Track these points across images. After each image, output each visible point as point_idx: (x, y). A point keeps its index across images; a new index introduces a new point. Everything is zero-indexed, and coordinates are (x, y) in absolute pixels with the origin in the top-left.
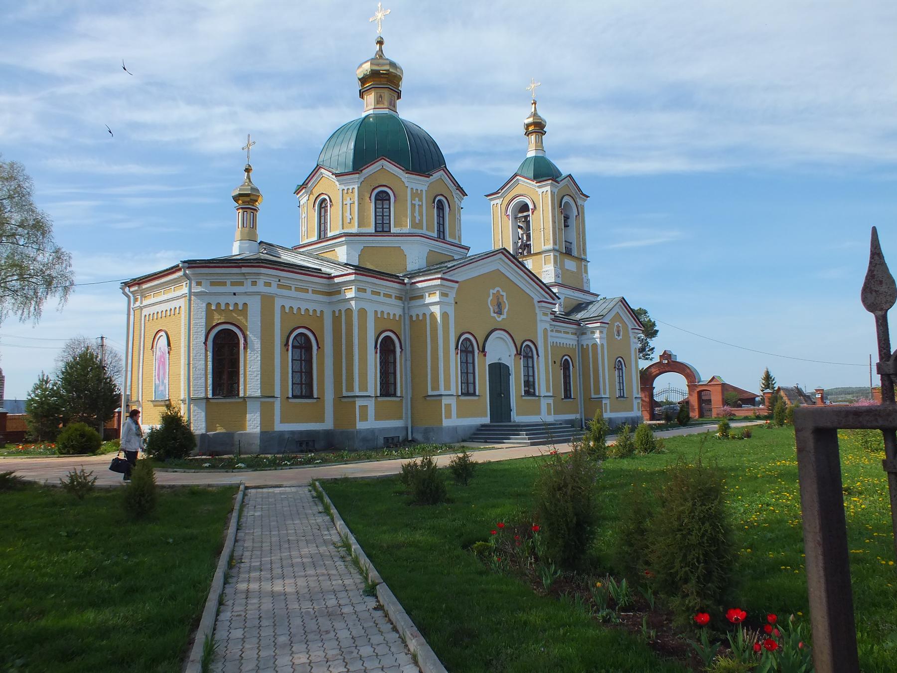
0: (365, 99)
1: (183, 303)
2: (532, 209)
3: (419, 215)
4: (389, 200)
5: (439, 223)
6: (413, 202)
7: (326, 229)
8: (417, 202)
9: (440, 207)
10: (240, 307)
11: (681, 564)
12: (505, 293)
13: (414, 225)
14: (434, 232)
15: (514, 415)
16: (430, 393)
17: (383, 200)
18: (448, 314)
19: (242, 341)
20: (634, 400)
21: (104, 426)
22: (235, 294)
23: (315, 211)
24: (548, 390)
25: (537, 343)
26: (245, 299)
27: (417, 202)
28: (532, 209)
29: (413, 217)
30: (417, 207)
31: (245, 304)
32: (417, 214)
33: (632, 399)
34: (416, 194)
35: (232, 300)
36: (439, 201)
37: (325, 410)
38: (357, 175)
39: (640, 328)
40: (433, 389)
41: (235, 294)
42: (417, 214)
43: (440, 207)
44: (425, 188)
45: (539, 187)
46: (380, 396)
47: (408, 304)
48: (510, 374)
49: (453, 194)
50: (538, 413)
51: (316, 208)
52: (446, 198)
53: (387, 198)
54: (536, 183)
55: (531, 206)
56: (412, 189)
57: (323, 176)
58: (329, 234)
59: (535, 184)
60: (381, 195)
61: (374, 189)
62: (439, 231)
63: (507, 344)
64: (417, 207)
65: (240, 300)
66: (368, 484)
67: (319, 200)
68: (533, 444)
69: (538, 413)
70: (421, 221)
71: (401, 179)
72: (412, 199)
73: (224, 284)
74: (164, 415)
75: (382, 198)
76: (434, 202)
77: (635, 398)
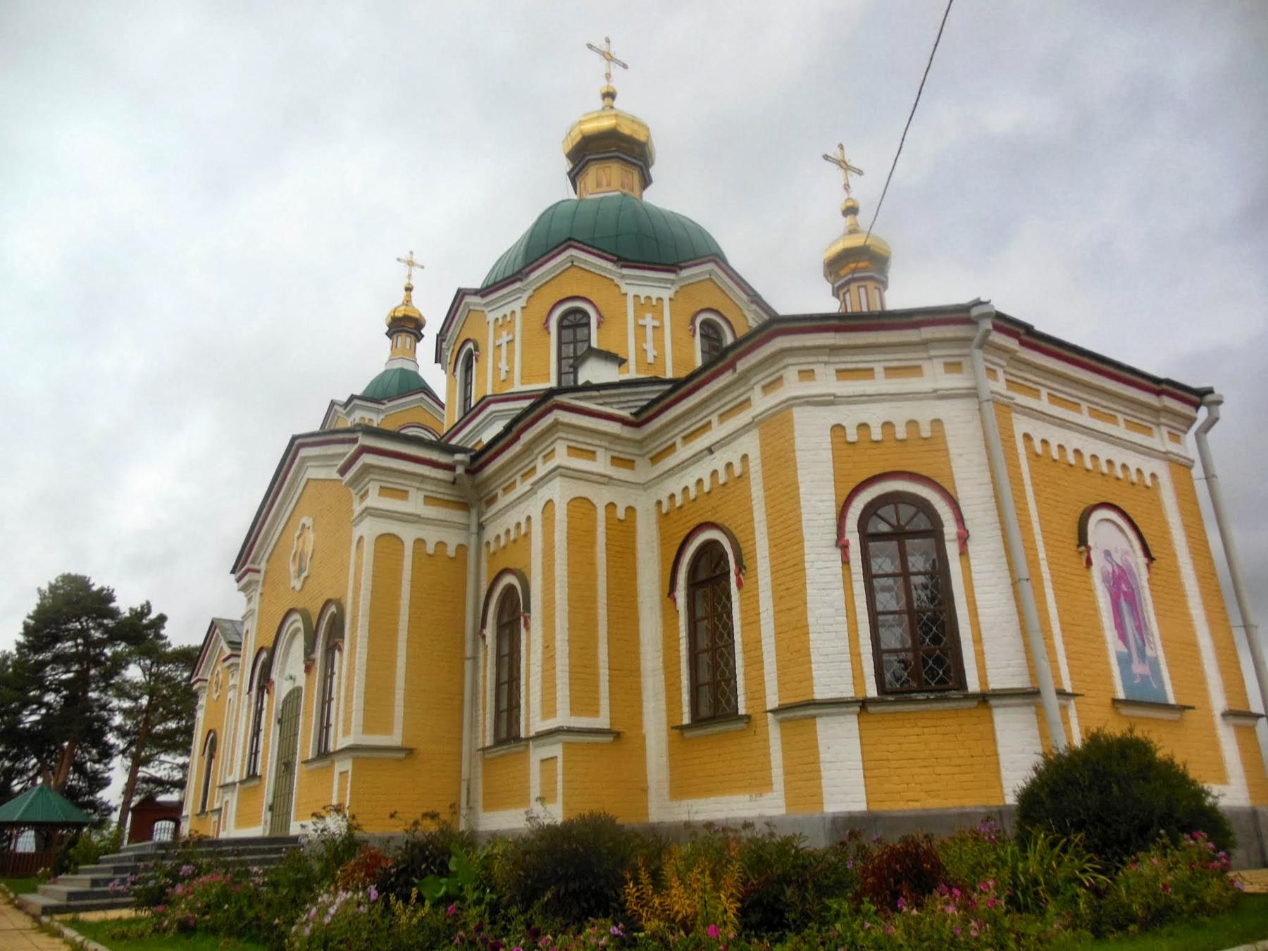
0: (395, 340)
1: (750, 444)
3: (655, 348)
4: (588, 325)
6: (641, 322)
8: (649, 321)
11: (1197, 898)
17: (575, 326)
21: (184, 767)
24: (376, 715)
25: (956, 492)
27: (649, 321)
29: (496, 369)
30: (649, 331)
31: (937, 423)
32: (649, 346)
34: (644, 306)
35: (899, 414)
37: (949, 439)
42: (649, 346)
44: (666, 294)
47: (480, 514)
53: (584, 321)
56: (636, 296)
57: (470, 311)
64: (649, 331)
65: (924, 413)
66: (728, 702)
67: (463, 353)
68: (804, 848)
71: (612, 280)
72: (637, 316)
73: (868, 373)
75: (574, 323)
76: (693, 322)
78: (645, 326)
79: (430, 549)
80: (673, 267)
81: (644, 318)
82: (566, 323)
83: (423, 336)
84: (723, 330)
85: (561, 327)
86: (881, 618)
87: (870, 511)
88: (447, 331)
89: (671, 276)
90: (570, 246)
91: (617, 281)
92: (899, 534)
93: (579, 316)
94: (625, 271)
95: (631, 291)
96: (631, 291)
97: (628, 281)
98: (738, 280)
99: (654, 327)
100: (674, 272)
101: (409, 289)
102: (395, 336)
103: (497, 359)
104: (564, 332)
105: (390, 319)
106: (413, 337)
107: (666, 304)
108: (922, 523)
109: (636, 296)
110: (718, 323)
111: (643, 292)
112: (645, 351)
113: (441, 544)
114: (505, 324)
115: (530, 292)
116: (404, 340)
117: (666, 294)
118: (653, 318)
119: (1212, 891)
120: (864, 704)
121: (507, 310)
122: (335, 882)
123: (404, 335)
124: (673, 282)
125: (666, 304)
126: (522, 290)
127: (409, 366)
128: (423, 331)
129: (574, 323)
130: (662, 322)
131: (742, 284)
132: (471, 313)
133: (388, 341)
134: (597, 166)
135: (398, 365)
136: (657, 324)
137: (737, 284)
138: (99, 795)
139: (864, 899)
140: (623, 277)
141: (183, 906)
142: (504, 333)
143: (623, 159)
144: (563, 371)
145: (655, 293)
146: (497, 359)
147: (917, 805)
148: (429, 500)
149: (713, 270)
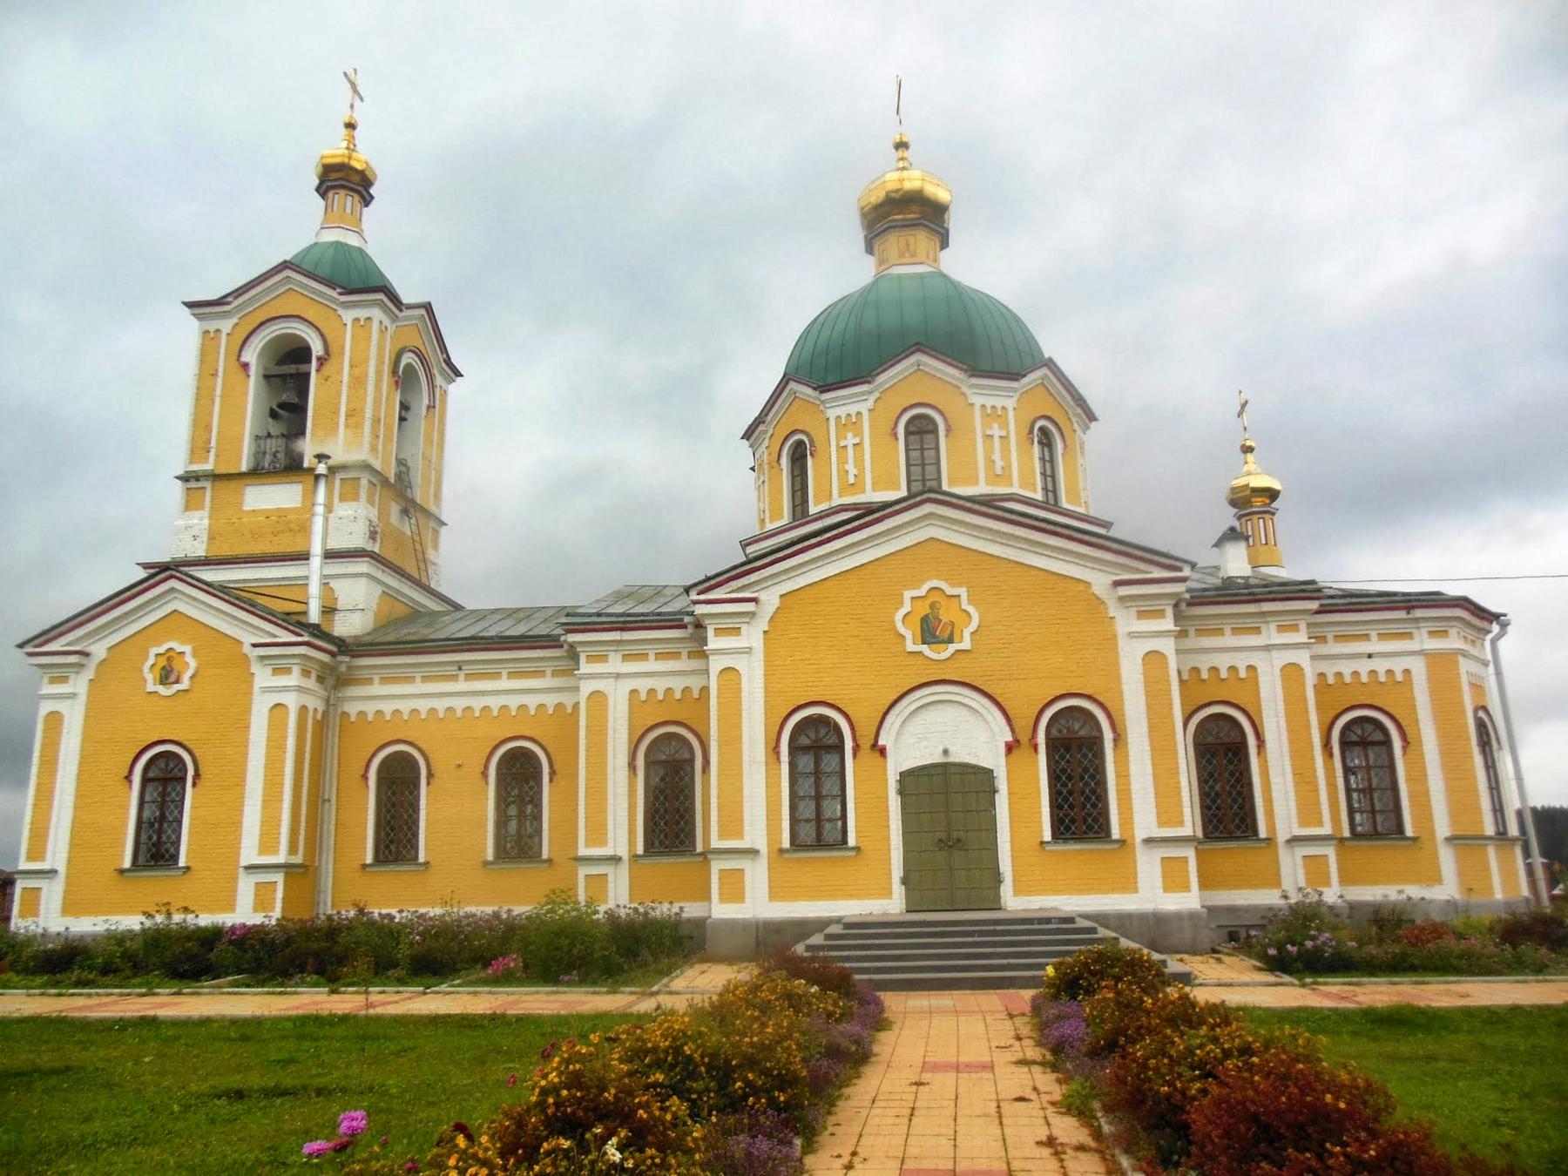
0: (330, 199)
2: (319, 359)
5: (1044, 474)
7: (805, 501)
8: (996, 431)
9: (1046, 440)
10: (1399, 677)
12: (965, 589)
13: (994, 478)
14: (1035, 491)
15: (1006, 890)
16: (583, 851)
17: (921, 433)
18: (1157, 652)
19: (1108, 735)
20: (241, 873)
22: (1370, 656)
23: (423, 453)
25: (1260, 712)
26: (1256, 659)
27: (996, 431)
28: (319, 359)
30: (997, 441)
32: (997, 457)
33: (237, 869)
36: (1043, 430)
38: (865, 388)
39: (299, 639)
40: (30, 858)
41: (1370, 656)
42: (997, 457)
43: (1046, 440)
44: (864, 408)
45: (346, 305)
46: (644, 856)
48: (995, 791)
49: (1071, 415)
50: (1129, 883)
51: (785, 461)
52: (905, 410)
54: (340, 294)
55: (317, 349)
57: (795, 397)
58: (813, 509)
59: (337, 297)
60: (917, 422)
61: (905, 410)
62: (1045, 489)
63: (982, 716)
64: (997, 441)
65: (1398, 666)
69: (1129, 883)
70: (1007, 467)
72: (985, 426)
74: (404, 921)
75: (921, 430)
76: (1031, 432)
77: (247, 868)
78: (992, 436)
79: (643, 697)
80: (1015, 376)
81: (991, 428)
82: (912, 429)
83: (372, 197)
84: (1053, 435)
85: (908, 433)
86: (1379, 828)
87: (1348, 727)
88: (767, 415)
89: (1014, 385)
90: (918, 350)
91: (965, 389)
92: (1364, 743)
93: (924, 422)
94: (975, 381)
95: (978, 401)
96: (978, 401)
97: (975, 391)
98: (1067, 383)
99: (1001, 437)
100: (1016, 380)
101: (351, 126)
102: (330, 194)
103: (842, 461)
104: (912, 438)
105: (320, 169)
106: (357, 198)
107: (1011, 414)
108: (1378, 736)
109: (983, 406)
110: (1051, 431)
111: (989, 402)
112: (994, 462)
113: (686, 690)
114: (852, 424)
115: (877, 395)
116: (345, 201)
117: (1010, 403)
118: (1000, 428)
119: (1203, 1081)
120: (1199, 842)
121: (853, 409)
122: (709, 1068)
123: (342, 192)
124: (1015, 390)
125: (1011, 414)
126: (870, 392)
127: (353, 240)
128: (372, 191)
129: (921, 430)
130: (1008, 432)
131: (1071, 388)
132: (797, 400)
133: (319, 203)
134: (898, 234)
135: (330, 236)
136: (1004, 433)
137: (1059, 380)
138: (878, 993)
139: (611, 1098)
140: (973, 386)
141: (579, 1094)
142: (850, 435)
143: (930, 228)
144: (913, 478)
145: (853, 409)
146: (842, 461)
147: (665, 861)
148: (555, 674)
149: (1046, 375)
